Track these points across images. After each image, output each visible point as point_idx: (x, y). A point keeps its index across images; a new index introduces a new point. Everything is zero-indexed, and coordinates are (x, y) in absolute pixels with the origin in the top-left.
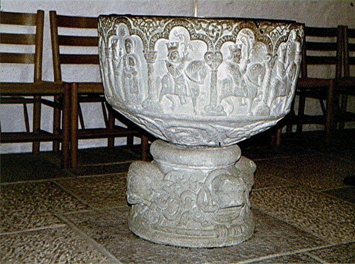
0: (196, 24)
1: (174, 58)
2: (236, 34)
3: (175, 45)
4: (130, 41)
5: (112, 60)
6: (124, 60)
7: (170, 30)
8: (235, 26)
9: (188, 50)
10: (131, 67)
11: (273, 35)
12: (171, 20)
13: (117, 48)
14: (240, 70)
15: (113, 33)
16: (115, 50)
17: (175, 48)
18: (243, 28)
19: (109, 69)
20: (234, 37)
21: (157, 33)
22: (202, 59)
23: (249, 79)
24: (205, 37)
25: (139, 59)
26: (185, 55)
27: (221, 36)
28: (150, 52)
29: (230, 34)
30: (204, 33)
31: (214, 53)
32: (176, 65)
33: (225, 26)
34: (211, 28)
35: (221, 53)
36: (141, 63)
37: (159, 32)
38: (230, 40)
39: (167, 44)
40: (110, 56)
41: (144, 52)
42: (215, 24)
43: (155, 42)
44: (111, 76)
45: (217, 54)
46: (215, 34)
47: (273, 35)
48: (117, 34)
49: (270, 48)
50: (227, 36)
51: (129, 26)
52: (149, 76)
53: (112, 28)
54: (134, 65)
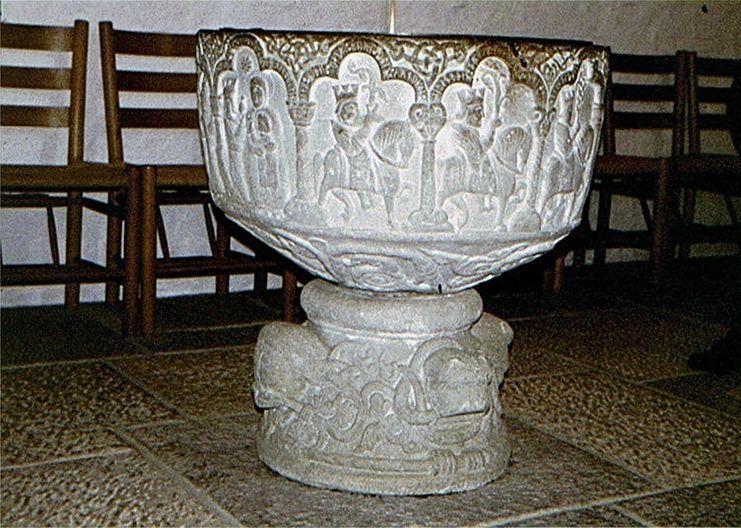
0: (392, 47)
1: (349, 116)
2: (473, 68)
3: (350, 90)
4: (260, 82)
5: (225, 121)
6: (248, 119)
7: (340, 61)
8: (470, 52)
9: (378, 100)
10: (261, 135)
11: (547, 71)
12: (343, 40)
13: (235, 96)
14: (481, 140)
15: (226, 65)
16: (231, 100)
17: (351, 96)
18: (487, 56)
19: (218, 137)
20: (469, 74)
21: (314, 65)
22: (405, 118)
23: (498, 158)
24: (410, 74)
25: (278, 118)
26: (371, 110)
27: (442, 72)
28: (301, 105)
29: (461, 67)
30: (409, 66)
31: (429, 105)
32: (353, 129)
33: (450, 52)
34: (422, 56)
35: (442, 106)
36: (283, 126)
37: (319, 64)
38: (461, 81)
39: (335, 89)
40: (221, 112)
41: (288, 103)
42: (430, 48)
43: (310, 84)
44: (223, 152)
45: (436, 109)
46: (431, 68)
47: (547, 71)
48: (235, 67)
49: (541, 97)
50: (455, 73)
51: (259, 52)
52: (298, 151)
53: (224, 55)
54: (268, 131)
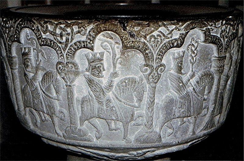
11: (153, 39)
29: (84, 38)
30: (52, 38)
34: (58, 31)
38: (84, 47)
42: (62, 26)
45: (70, 65)
46: (64, 38)
49: (146, 57)
50: (79, 42)
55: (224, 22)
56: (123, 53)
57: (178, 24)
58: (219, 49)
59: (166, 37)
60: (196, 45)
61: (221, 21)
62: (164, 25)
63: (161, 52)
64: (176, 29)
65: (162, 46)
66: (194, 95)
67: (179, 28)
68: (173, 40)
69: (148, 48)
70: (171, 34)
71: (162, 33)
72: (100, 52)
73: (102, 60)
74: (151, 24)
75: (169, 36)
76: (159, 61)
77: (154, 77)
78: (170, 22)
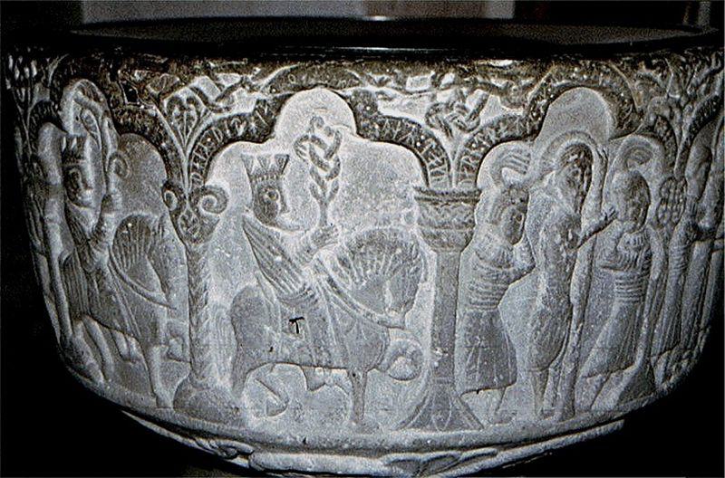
11: (176, 111)
55: (449, 77)
56: (122, 145)
57: (250, 71)
58: (428, 165)
59: (213, 105)
60: (330, 141)
61: (433, 73)
62: (208, 71)
63: (198, 151)
64: (244, 87)
65: (202, 134)
66: (336, 301)
67: (254, 83)
68: (234, 116)
69: (166, 134)
70: (226, 101)
71: (201, 93)
72: (79, 135)
73: (79, 157)
74: (174, 66)
75: (221, 104)
76: (198, 177)
77: (190, 222)
78: (226, 63)
